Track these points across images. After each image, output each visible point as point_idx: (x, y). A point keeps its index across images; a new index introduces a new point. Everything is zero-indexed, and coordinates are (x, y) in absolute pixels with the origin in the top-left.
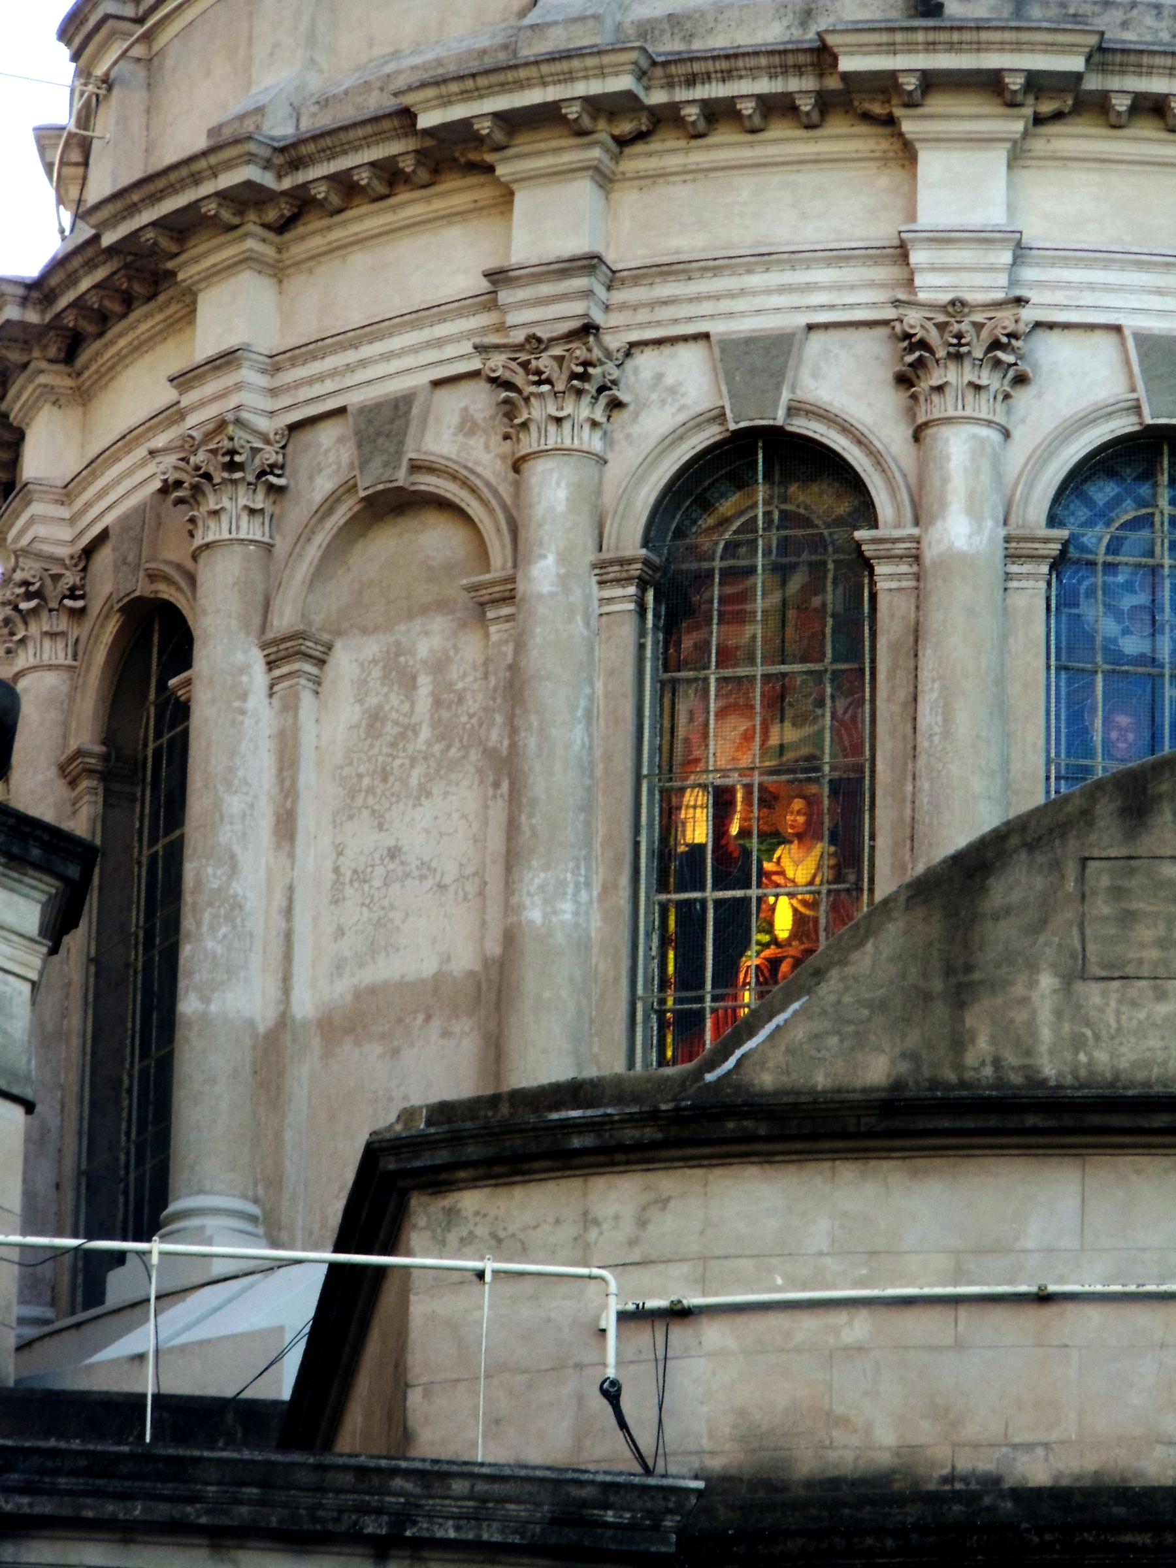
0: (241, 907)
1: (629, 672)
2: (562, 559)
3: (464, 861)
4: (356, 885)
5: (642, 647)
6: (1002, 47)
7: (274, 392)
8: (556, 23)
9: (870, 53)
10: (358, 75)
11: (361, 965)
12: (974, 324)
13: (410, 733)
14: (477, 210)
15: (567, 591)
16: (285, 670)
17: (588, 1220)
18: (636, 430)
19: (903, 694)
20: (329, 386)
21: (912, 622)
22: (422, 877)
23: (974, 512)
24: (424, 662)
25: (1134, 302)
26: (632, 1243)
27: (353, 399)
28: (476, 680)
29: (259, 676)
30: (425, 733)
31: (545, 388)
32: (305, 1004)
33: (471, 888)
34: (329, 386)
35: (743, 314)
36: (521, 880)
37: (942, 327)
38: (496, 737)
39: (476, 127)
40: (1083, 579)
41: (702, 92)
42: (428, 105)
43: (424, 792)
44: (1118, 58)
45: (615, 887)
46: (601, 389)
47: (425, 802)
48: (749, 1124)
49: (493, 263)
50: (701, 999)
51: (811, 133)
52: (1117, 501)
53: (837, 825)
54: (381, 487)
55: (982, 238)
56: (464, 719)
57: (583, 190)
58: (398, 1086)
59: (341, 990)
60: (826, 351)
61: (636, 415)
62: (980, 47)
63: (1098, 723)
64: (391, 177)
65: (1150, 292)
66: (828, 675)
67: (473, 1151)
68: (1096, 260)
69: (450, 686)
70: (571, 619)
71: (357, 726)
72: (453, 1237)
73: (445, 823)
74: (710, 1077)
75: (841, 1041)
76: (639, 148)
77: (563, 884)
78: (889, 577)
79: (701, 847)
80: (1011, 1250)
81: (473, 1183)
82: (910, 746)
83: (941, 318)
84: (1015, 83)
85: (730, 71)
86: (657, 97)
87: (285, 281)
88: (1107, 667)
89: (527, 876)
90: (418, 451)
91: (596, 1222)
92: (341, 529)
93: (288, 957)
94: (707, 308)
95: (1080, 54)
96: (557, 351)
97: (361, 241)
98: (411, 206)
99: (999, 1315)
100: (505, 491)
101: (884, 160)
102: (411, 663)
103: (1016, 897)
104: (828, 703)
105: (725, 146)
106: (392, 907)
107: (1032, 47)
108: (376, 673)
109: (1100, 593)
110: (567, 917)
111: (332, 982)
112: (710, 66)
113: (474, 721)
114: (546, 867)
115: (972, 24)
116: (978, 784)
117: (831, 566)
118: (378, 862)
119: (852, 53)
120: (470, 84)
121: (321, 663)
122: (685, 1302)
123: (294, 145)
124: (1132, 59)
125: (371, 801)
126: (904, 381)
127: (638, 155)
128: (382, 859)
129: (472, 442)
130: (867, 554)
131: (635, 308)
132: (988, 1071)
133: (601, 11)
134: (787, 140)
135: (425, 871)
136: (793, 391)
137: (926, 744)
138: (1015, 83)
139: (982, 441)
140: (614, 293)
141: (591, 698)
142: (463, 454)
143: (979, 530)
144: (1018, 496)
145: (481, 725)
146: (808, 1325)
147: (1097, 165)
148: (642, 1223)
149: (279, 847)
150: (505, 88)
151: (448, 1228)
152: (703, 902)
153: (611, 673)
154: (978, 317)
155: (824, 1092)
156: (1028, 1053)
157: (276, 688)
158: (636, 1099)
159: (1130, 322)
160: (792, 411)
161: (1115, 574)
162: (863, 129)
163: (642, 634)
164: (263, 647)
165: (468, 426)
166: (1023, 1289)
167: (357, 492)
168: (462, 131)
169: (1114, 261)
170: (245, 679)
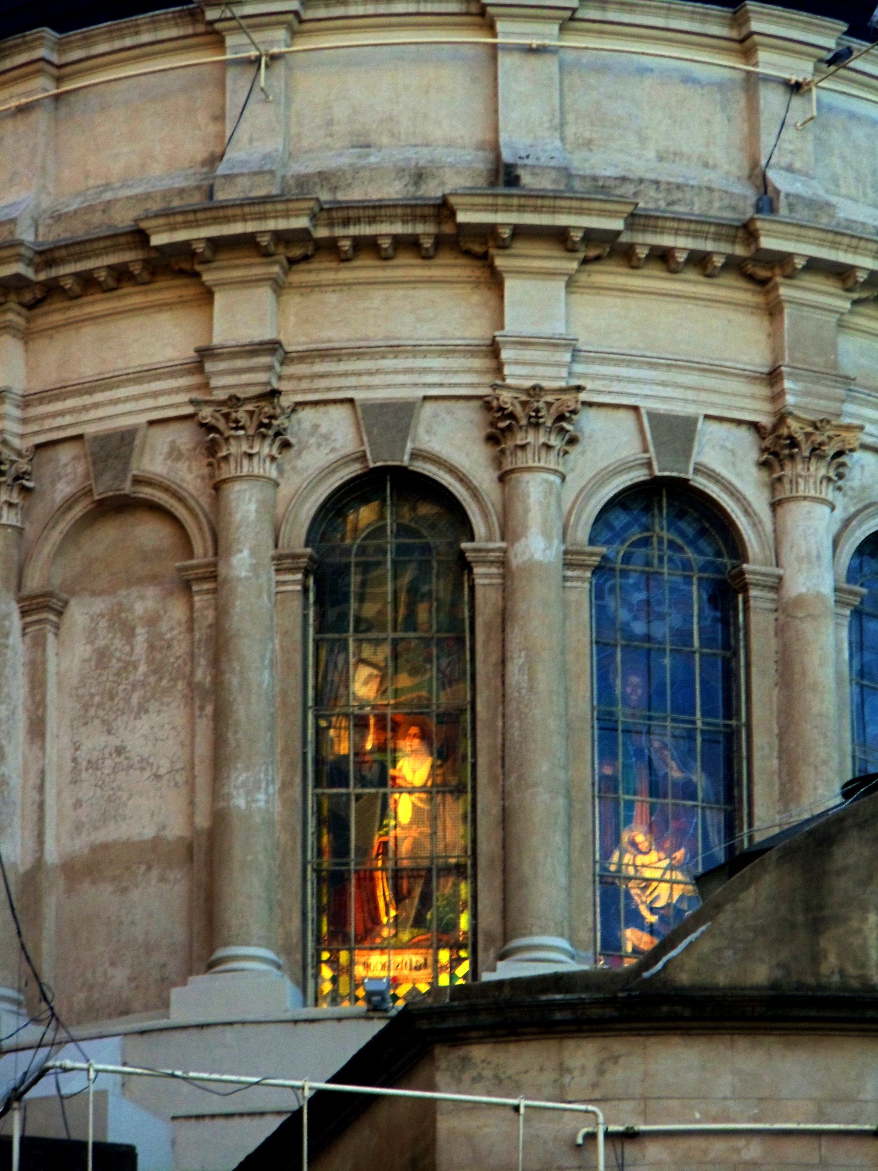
0: (8, 784)
1: (298, 634)
2: (252, 554)
3: (175, 759)
4: (90, 771)
5: (305, 617)
6: (570, 211)
7: (25, 421)
8: (242, 175)
9: (480, 211)
10: (79, 200)
11: (96, 828)
12: (547, 403)
13: (131, 668)
14: (182, 303)
15: (257, 576)
16: (35, 618)
17: (563, 1069)
18: (299, 463)
19: (494, 658)
20: (68, 419)
21: (500, 609)
22: (143, 769)
23: (547, 534)
24: (141, 618)
25: (647, 390)
26: (595, 1086)
27: (89, 430)
28: (180, 633)
29: (16, 622)
30: (142, 668)
31: (241, 432)
32: (52, 854)
33: (181, 778)
34: (68, 419)
35: (377, 387)
36: (228, 777)
37: (524, 404)
38: (202, 675)
39: (194, 246)
40: (606, 580)
41: (354, 230)
42: (159, 230)
43: (143, 709)
44: (642, 221)
45: (291, 783)
46: (278, 434)
47: (144, 716)
48: (678, 1009)
49: (202, 343)
50: (347, 864)
51: (427, 262)
52: (627, 527)
53: (442, 746)
54: (111, 494)
55: (552, 343)
56: (172, 660)
57: (265, 293)
58: (127, 914)
59: (80, 845)
60: (436, 415)
61: (299, 454)
62: (554, 210)
63: (619, 681)
64: (122, 276)
65: (657, 384)
66: (434, 641)
67: (484, 1018)
68: (623, 361)
69: (161, 636)
70: (260, 596)
71: (89, 660)
72: (467, 1076)
73: (159, 733)
74: (646, 975)
75: (735, 954)
76: (302, 266)
77: (258, 782)
78: (484, 575)
79: (346, 757)
80: (854, 1100)
81: (480, 1041)
82: (500, 694)
83: (524, 398)
84: (577, 236)
85: (375, 217)
86: (322, 233)
87: (30, 343)
88: (623, 642)
89: (234, 775)
90: (138, 469)
91: (569, 1071)
92: (77, 522)
93: (41, 819)
94: (352, 381)
95: (620, 218)
96: (250, 407)
97: (93, 319)
98: (134, 298)
99: (849, 1144)
100: (204, 501)
101: (477, 284)
102: (130, 617)
103: (851, 860)
104: (435, 659)
105: (366, 269)
106: (119, 788)
107: (588, 212)
108: (103, 623)
109: (618, 591)
110: (262, 804)
111: (72, 839)
112: (361, 213)
113: (180, 661)
114: (247, 769)
115: (551, 194)
116: (553, 724)
117: (435, 565)
118: (107, 756)
119: (466, 210)
120: (191, 217)
121: (60, 614)
122: (636, 1128)
123: (50, 250)
124: (652, 222)
125: (101, 713)
126: (493, 439)
127: (303, 271)
128: (111, 755)
129: (179, 465)
130: (469, 559)
131: (300, 378)
132: (836, 978)
133: (274, 168)
134: (411, 266)
135: (144, 764)
136: (413, 441)
137: (516, 694)
138: (577, 236)
139: (551, 484)
140: (285, 368)
141: (273, 651)
142: (172, 474)
143: (549, 547)
144: (571, 523)
145: (185, 664)
146: (719, 1147)
147: (619, 293)
148: (601, 1072)
149: (32, 742)
150: (216, 221)
151: (463, 1070)
152: (348, 795)
153: (285, 634)
154: (549, 398)
155: (724, 988)
156: (863, 966)
157: (27, 631)
158: (598, 988)
159: (645, 405)
160: (414, 456)
161: (628, 577)
162: (466, 261)
163: (306, 607)
164: (19, 601)
165: (175, 454)
166: (867, 1127)
167: (92, 495)
168: (184, 249)
169: (635, 361)
170: (7, 623)
